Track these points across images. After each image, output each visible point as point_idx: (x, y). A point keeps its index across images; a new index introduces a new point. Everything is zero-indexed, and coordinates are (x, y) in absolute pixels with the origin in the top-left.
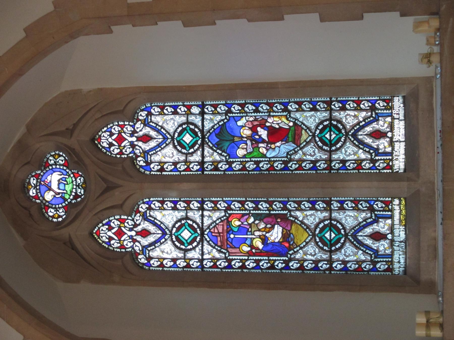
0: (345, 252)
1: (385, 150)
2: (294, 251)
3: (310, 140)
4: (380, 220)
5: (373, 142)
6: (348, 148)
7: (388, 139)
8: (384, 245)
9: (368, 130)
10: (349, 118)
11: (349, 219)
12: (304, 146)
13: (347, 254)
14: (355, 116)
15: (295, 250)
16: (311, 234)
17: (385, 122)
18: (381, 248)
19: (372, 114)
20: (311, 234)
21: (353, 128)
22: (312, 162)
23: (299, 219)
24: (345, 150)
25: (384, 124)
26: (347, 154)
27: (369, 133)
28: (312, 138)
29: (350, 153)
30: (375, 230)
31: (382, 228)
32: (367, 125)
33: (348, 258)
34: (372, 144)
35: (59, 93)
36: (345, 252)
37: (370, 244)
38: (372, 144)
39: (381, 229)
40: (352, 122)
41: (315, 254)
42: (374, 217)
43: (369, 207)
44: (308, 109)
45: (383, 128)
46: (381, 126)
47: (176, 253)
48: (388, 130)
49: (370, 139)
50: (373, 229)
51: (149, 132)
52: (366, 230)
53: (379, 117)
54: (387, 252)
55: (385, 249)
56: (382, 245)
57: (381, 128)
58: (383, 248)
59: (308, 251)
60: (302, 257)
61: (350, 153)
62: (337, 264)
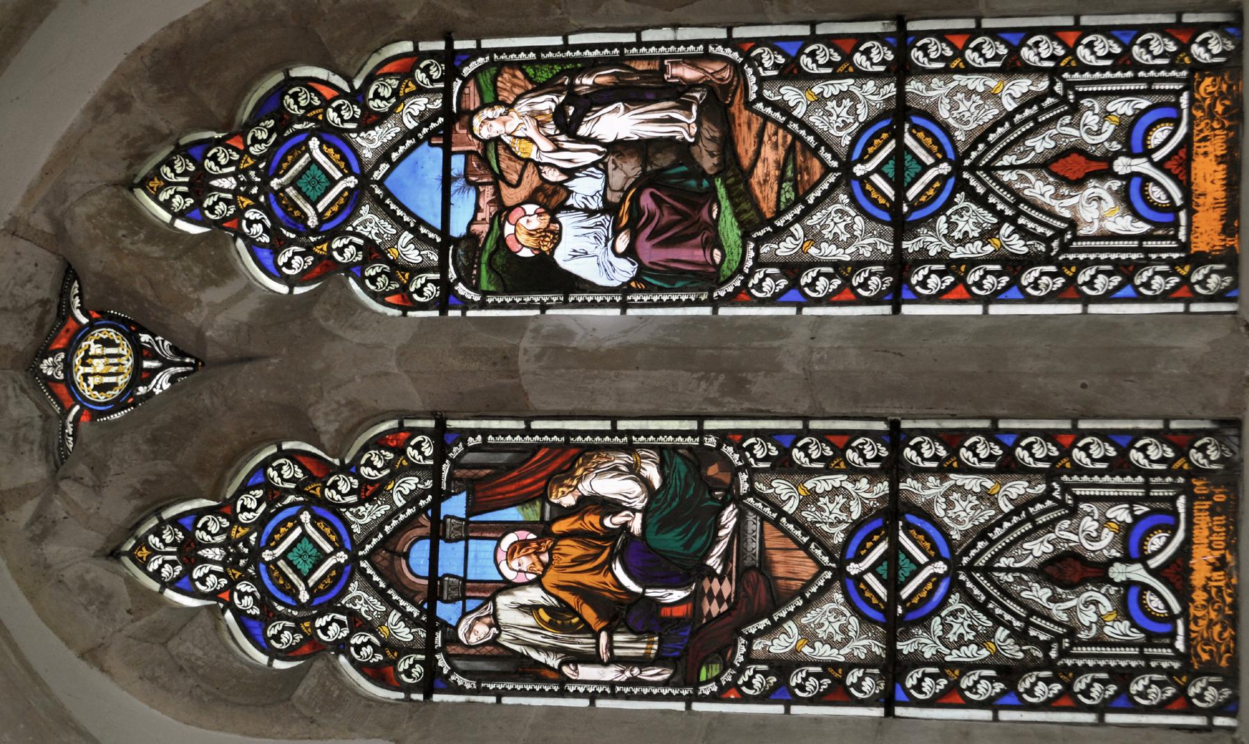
2: (774, 227)
4: (1084, 507)
7: (1116, 184)
8: (1096, 603)
11: (964, 103)
14: (989, 95)
15: (780, 223)
16: (835, 164)
17: (1104, 522)
18: (1088, 617)
19: (1050, 490)
22: (828, 667)
23: (795, 113)
24: (948, 221)
25: (1100, 124)
30: (1064, 547)
31: (1090, 538)
35: (64, 129)
37: (1047, 200)
38: (1054, 203)
39: (1085, 137)
45: (1097, 546)
46: (1090, 538)
48: (1116, 146)
52: (1026, 546)
53: (1080, 96)
54: (1107, 630)
55: (1101, 622)
57: (1088, 139)
58: (1094, 618)
59: (825, 226)
61: (961, 636)
62: (926, 272)
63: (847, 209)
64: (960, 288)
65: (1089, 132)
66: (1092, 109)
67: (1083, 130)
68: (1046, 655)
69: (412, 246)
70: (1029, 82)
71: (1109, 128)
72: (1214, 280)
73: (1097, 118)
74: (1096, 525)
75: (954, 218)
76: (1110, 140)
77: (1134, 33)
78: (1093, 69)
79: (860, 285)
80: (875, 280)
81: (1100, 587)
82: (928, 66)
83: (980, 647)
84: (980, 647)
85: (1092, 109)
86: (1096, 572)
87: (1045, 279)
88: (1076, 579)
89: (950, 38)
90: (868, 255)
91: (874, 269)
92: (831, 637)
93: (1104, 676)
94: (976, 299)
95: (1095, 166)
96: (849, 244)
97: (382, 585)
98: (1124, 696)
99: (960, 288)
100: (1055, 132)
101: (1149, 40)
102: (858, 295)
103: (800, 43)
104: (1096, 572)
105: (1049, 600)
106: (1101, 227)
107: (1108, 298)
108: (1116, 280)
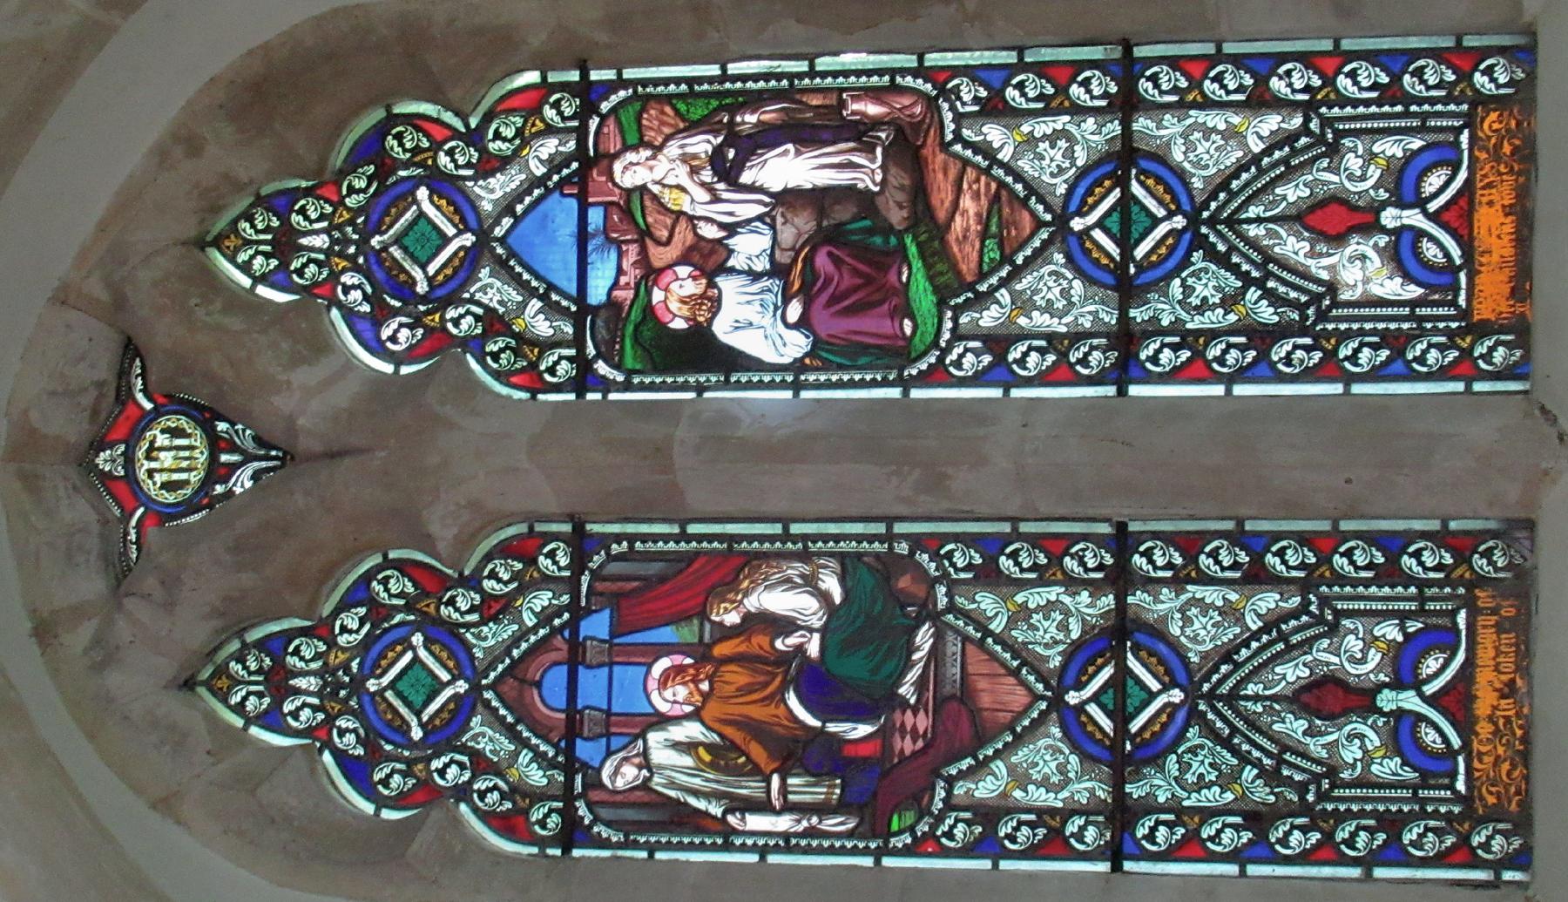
0: (1069, 154)
1: (1365, 291)
3: (497, 222)
5: (1312, 254)
7: (1383, 240)
8: (1362, 737)
10: (1201, 145)
12: (1236, 175)
13: (1062, 144)
18: (1351, 753)
21: (1038, 253)
26: (1195, 301)
27: (1294, 211)
28: (1052, 235)
29: (1205, 299)
30: (1321, 671)
32: (1290, 172)
33: (1059, 127)
34: (1309, 262)
36: (1069, 154)
40: (1217, 163)
41: (1066, 782)
43: (988, 99)
44: (1033, 105)
47: (480, 746)
49: (1300, 238)
51: (1312, 254)
53: (1339, 135)
58: (1359, 755)
60: (1005, 795)
61: (1205, 299)
65: (1350, 177)
70: (1280, 118)
78: (1355, 103)
81: (1365, 719)
85: (1354, 150)
86: (1361, 700)
90: (1088, 325)
95: (1358, 219)
104: (1361, 700)
105: (1305, 733)
106: (1365, 291)
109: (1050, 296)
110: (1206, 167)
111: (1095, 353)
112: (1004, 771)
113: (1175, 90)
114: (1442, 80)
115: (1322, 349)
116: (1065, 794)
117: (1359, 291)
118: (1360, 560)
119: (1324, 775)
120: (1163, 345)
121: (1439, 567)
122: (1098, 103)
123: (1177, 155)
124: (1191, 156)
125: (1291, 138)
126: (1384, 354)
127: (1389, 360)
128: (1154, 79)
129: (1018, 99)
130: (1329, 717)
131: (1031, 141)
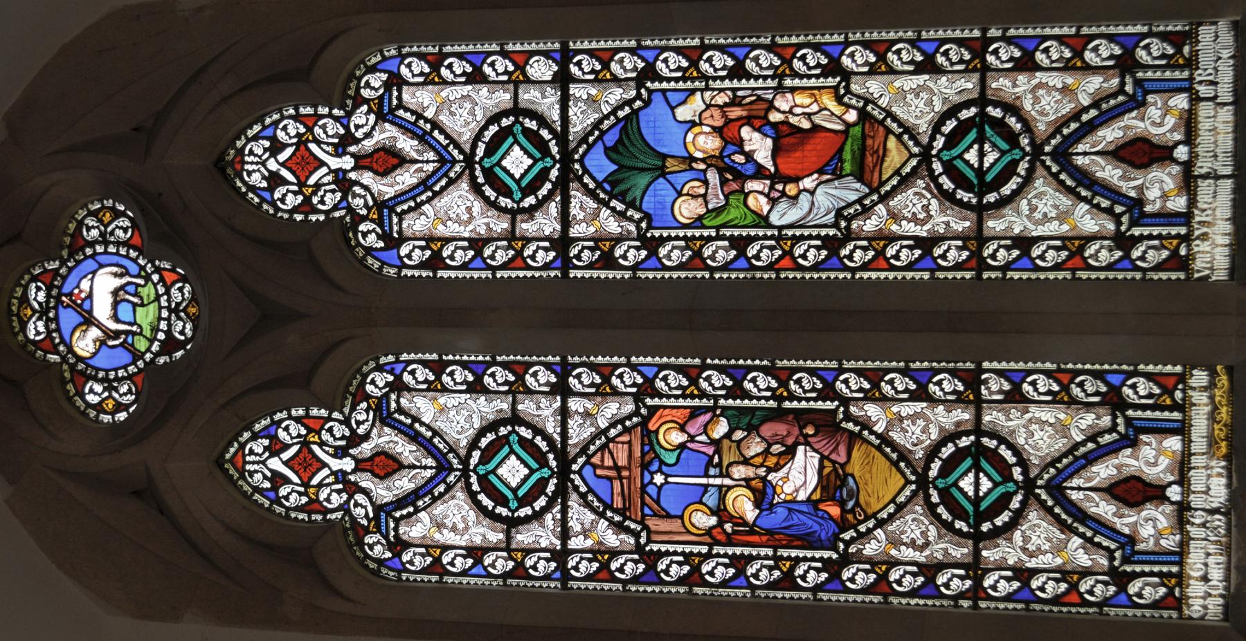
4: (1144, 437)
6: (1040, 196)
8: (1154, 520)
9: (1109, 139)
18: (1146, 531)
19: (1123, 84)
20: (913, 478)
30: (1127, 472)
31: (1148, 464)
41: (927, 544)
42: (1121, 428)
45: (1161, 130)
50: (1119, 468)
54: (1163, 542)
56: (1147, 520)
57: (1154, 131)
58: (1152, 532)
63: (924, 192)
64: (479, 260)
65: (1154, 124)
66: (1155, 104)
67: (1147, 123)
68: (637, 542)
69: (1088, 216)
70: (1101, 79)
71: (1170, 121)
72: (721, 255)
73: (1159, 112)
74: (1154, 452)
75: (1034, 201)
76: (1172, 130)
77: (1038, 40)
78: (669, 80)
79: (940, 256)
80: (676, 253)
81: (1157, 507)
82: (855, 70)
83: (586, 537)
84: (586, 537)
85: (1155, 104)
86: (1156, 493)
87: (1151, 252)
88: (1139, 498)
89: (732, 50)
90: (942, 231)
91: (500, 243)
92: (913, 541)
93: (819, 565)
94: (489, 267)
95: (366, 162)
96: (469, 222)
97: (1050, 503)
98: (652, 572)
99: (479, 260)
100: (1122, 124)
101: (1049, 47)
102: (662, 264)
103: (657, 52)
104: (1156, 493)
105: (1114, 514)
106: (1163, 207)
107: (504, 267)
108: (1016, 253)
109: (914, 210)
110: (1047, 115)
111: (675, 251)
112: (883, 536)
113: (593, 71)
114: (1061, 57)
115: (513, 249)
116: (927, 552)
117: (1158, 205)
118: (459, 379)
119: (1126, 544)
120: (1000, 246)
121: (592, 385)
122: (907, 68)
123: (1027, 105)
124: (1037, 107)
125: (629, 102)
126: (918, 252)
127: (921, 257)
128: (579, 64)
129: (1145, 58)
130: (1131, 505)
131: (902, 92)
